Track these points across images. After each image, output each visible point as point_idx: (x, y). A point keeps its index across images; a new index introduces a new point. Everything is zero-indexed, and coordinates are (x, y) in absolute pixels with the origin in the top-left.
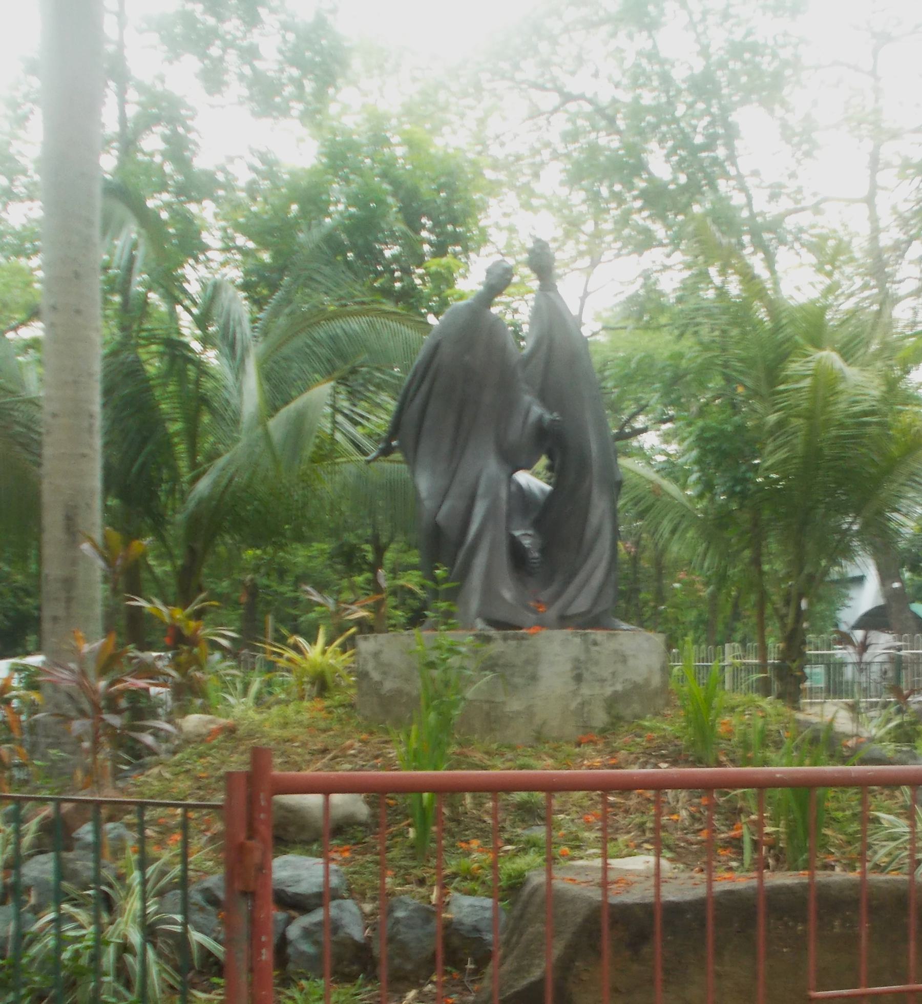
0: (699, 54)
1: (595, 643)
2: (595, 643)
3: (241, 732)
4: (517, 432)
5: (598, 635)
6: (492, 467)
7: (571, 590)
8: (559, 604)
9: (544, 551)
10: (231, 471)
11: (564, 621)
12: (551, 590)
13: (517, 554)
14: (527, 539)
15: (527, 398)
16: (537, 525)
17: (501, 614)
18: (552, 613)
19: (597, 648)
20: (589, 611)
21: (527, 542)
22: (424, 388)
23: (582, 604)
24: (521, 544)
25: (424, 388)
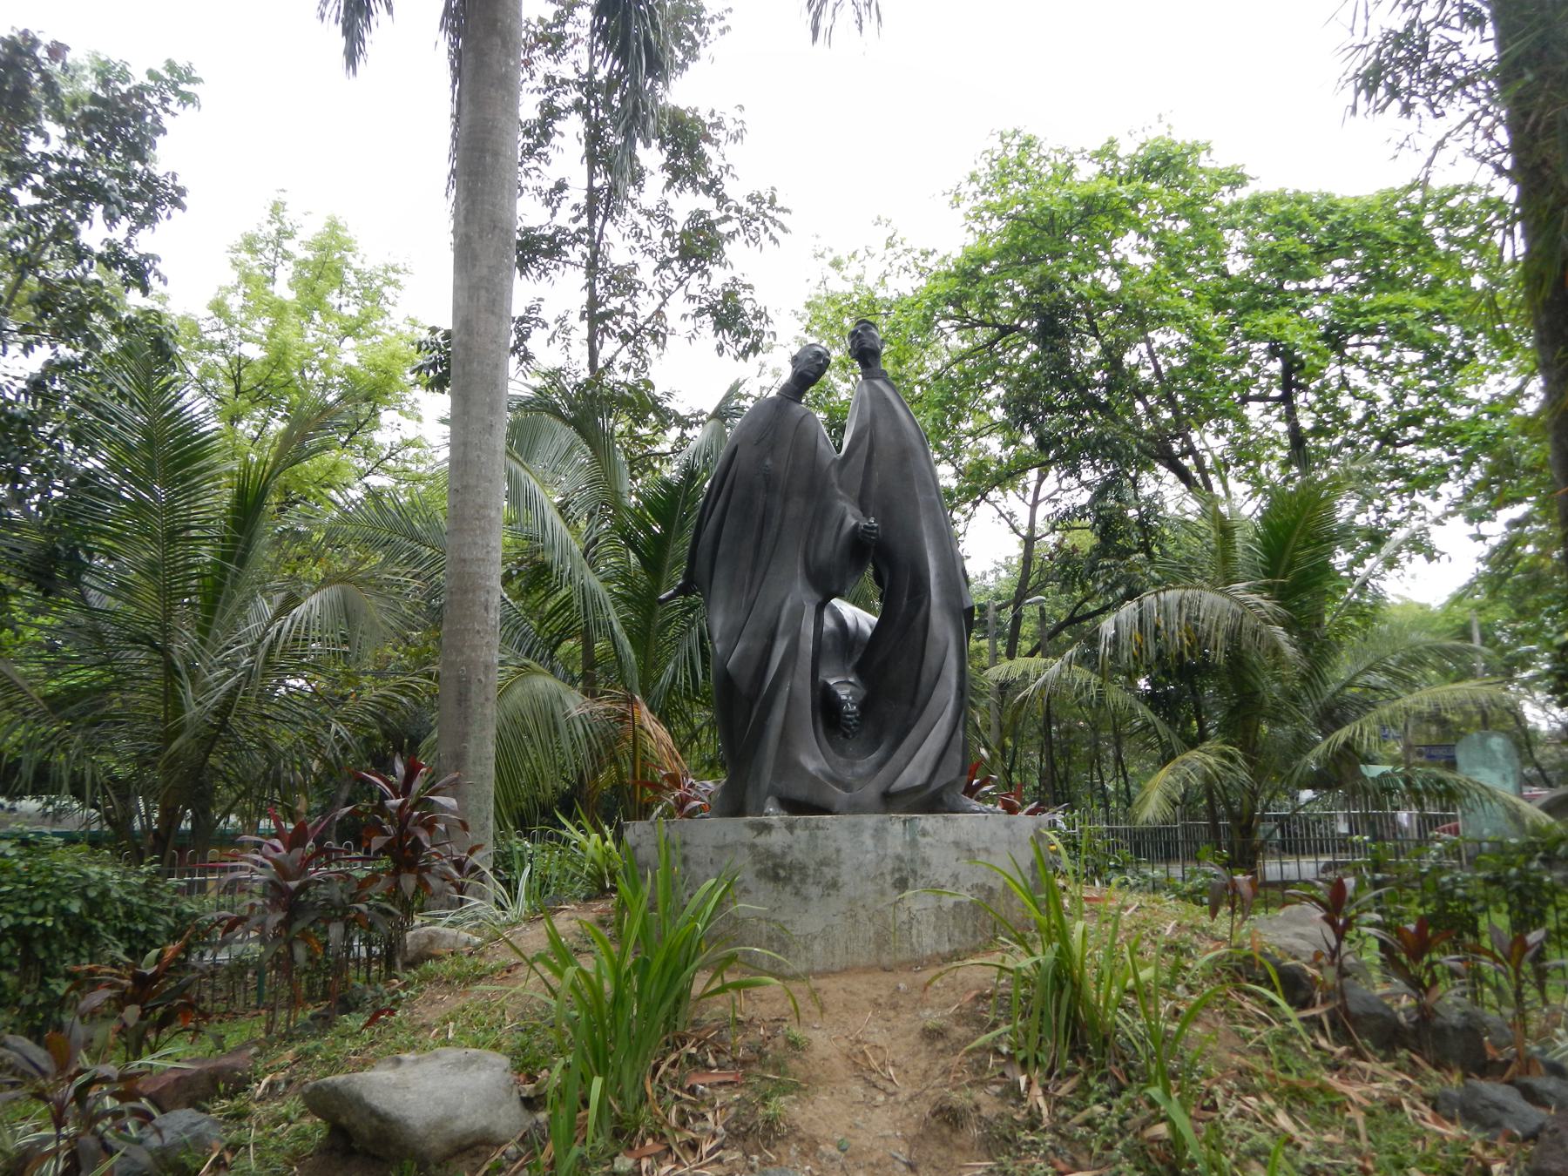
0: (746, 359)
1: (924, 833)
2: (924, 833)
3: (457, 485)
4: (829, 547)
5: (928, 821)
6: (799, 594)
7: (900, 754)
8: (883, 774)
9: (865, 706)
10: (1171, 916)
11: (890, 801)
12: (875, 757)
13: (826, 704)
14: (846, 690)
15: (841, 504)
16: (860, 670)
17: (800, 792)
18: (872, 790)
19: (928, 839)
20: (927, 784)
21: (844, 693)
22: (720, 504)
23: (914, 773)
24: (835, 693)
25: (720, 504)
